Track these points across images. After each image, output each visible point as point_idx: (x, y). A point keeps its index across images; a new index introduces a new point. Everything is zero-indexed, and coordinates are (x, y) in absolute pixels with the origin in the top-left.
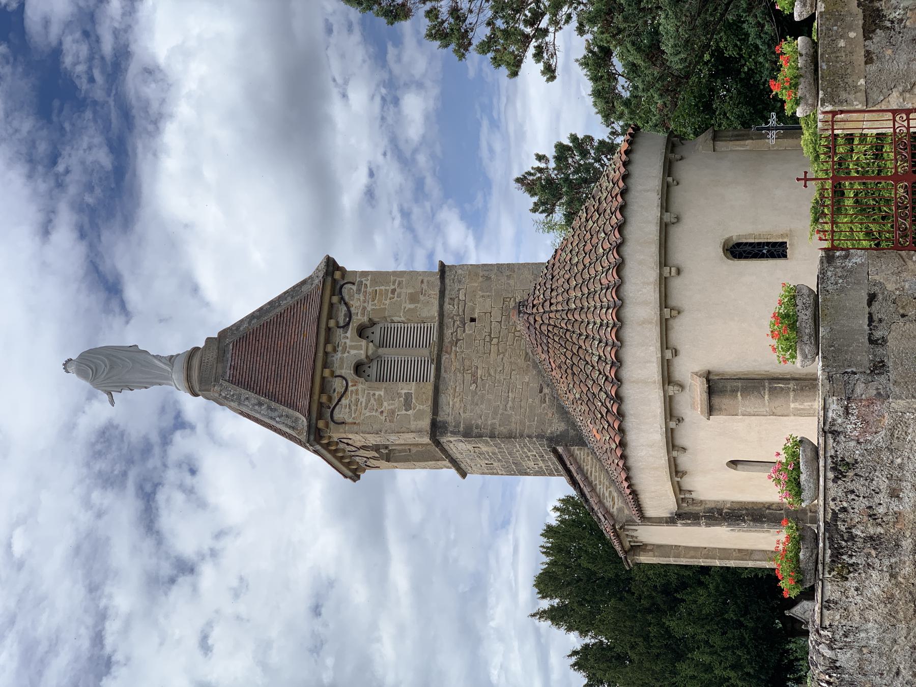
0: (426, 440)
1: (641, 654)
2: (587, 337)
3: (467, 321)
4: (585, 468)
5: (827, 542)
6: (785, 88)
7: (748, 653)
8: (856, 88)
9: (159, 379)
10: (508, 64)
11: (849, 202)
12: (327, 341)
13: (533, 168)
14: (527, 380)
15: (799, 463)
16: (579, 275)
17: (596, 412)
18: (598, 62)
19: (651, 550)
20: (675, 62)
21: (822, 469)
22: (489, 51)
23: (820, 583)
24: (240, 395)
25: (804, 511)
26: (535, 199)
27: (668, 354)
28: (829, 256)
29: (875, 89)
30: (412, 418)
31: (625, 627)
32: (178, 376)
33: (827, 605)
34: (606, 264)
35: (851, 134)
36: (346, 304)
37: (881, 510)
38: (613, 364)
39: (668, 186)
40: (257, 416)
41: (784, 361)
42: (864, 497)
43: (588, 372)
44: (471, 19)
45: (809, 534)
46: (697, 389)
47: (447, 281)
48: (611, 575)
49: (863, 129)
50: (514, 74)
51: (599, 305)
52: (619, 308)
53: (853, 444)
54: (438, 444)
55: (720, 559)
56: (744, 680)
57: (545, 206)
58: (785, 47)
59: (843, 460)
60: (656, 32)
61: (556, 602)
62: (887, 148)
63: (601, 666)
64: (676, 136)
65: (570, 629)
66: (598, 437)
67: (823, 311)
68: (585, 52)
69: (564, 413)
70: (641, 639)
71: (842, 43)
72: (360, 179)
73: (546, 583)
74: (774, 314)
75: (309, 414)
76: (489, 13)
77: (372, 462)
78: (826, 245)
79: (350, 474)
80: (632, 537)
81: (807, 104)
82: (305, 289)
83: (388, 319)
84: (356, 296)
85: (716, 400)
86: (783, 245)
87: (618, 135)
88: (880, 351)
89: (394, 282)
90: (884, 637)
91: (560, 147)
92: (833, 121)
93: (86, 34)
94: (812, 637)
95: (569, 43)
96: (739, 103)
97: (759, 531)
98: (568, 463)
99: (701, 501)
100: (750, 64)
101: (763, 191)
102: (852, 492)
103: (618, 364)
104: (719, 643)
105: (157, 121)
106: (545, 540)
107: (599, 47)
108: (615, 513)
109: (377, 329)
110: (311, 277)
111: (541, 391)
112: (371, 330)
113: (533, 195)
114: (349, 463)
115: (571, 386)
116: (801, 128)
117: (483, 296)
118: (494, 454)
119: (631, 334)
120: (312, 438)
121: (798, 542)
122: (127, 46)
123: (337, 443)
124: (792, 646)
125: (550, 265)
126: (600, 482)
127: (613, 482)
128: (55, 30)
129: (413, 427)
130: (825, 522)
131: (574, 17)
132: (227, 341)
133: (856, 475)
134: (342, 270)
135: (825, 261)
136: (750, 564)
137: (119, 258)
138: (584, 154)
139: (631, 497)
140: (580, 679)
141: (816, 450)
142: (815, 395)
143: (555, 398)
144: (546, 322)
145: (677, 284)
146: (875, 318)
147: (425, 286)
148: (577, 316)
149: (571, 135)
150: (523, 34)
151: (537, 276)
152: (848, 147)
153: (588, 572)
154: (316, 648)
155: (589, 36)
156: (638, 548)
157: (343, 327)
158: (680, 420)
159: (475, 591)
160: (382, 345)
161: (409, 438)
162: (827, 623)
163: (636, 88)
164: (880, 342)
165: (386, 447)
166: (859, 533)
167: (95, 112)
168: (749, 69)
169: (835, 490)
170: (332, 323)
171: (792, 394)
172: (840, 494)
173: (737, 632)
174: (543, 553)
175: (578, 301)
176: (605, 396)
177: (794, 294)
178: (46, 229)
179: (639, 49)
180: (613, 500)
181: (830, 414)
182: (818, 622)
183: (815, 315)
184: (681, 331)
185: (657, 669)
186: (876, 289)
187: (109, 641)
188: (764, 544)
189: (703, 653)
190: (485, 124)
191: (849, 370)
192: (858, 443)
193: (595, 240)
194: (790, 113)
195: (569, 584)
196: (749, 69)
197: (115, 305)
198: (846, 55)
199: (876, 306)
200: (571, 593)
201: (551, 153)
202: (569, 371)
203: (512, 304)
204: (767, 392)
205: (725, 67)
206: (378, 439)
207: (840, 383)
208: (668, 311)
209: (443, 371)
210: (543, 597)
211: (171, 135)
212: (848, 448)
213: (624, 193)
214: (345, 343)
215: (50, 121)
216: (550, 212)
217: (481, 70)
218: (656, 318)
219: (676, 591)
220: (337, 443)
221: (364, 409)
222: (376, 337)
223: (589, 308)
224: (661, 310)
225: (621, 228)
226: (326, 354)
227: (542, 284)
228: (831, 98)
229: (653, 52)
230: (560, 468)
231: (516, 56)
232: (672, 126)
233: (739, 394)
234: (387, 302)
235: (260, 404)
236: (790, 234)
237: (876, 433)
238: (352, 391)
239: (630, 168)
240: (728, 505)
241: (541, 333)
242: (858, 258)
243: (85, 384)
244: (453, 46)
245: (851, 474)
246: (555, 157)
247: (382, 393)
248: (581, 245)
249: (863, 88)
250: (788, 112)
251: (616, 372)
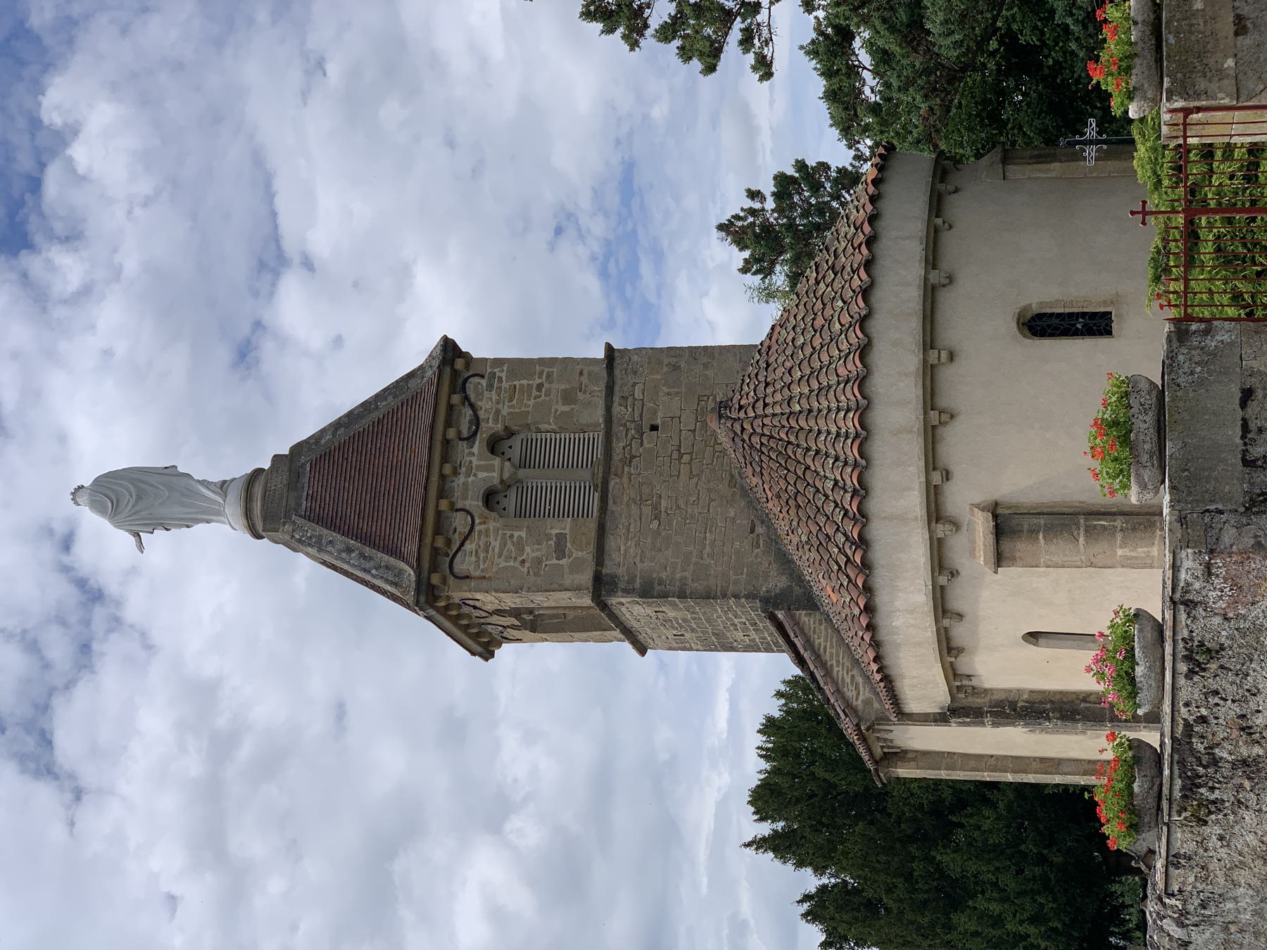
0: (587, 601)
1: (901, 901)
2: (817, 452)
3: (646, 429)
4: (817, 642)
5: (1176, 767)
6: (1112, 74)
7: (1055, 900)
8: (1221, 74)
10: (701, 55)
11: (1207, 248)
12: (445, 459)
13: (742, 209)
14: (732, 514)
15: (1133, 649)
16: (805, 362)
17: (832, 563)
18: (831, 49)
19: (913, 759)
21: (1168, 658)
22: (674, 38)
23: (1165, 828)
24: (320, 538)
26: (746, 254)
27: (936, 478)
28: (1180, 332)
29: (1250, 73)
30: (567, 570)
31: (878, 862)
32: (233, 509)
34: (844, 346)
35: (1210, 145)
36: (472, 406)
38: (855, 492)
39: (936, 231)
40: (346, 567)
41: (1111, 493)
42: (1233, 701)
43: (819, 505)
46: (982, 526)
47: (617, 372)
49: (1232, 136)
50: (710, 69)
51: (834, 405)
52: (863, 412)
53: (1217, 620)
54: (604, 607)
55: (1014, 772)
56: (1048, 938)
57: (759, 265)
59: (1201, 644)
61: (780, 825)
63: (845, 917)
64: (947, 158)
65: (800, 864)
66: (834, 597)
67: (1171, 415)
68: (814, 35)
69: (785, 562)
70: (901, 880)
73: (766, 799)
74: (1096, 421)
75: (419, 565)
77: (511, 633)
78: (1173, 313)
79: (479, 649)
80: (885, 740)
81: (1145, 98)
82: (413, 384)
83: (533, 428)
84: (486, 394)
85: (1006, 545)
86: (1107, 316)
87: (866, 161)
89: (541, 374)
90: (1262, 909)
91: (783, 181)
92: (1185, 124)
96: (1041, 111)
97: (1071, 733)
98: (792, 635)
99: (986, 690)
100: (1057, 55)
102: (1216, 693)
103: (863, 492)
104: (1013, 885)
106: (764, 739)
107: (835, 27)
108: (860, 708)
109: (516, 442)
110: (421, 368)
111: (752, 531)
112: (509, 442)
113: (742, 249)
114: (478, 635)
115: (795, 523)
116: (1133, 142)
117: (668, 394)
118: (685, 620)
119: (881, 448)
120: (422, 599)
121: (1131, 767)
123: (459, 606)
124: (1116, 888)
125: (763, 349)
126: (838, 661)
127: (856, 662)
129: (567, 582)
130: (1172, 738)
132: (303, 459)
133: (1222, 667)
134: (466, 356)
135: (1174, 340)
136: (1057, 779)
138: (816, 187)
139: (882, 684)
140: (815, 935)
142: (1153, 536)
143: (774, 541)
144: (759, 430)
145: (947, 374)
146: (1252, 426)
147: (584, 379)
148: (802, 423)
149: (797, 161)
151: (747, 364)
152: (1205, 169)
153: (821, 785)
156: (898, 755)
157: (467, 439)
158: (954, 574)
160: (523, 464)
162: (1176, 888)
163: (888, 85)
164: (1259, 463)
165: (531, 611)
166: (1225, 755)
168: (1056, 62)
169: (1188, 690)
170: (452, 433)
171: (1119, 536)
172: (1196, 696)
173: (1037, 871)
174: (761, 756)
175: (804, 401)
176: (843, 539)
179: (892, 29)
180: (857, 688)
181: (1183, 575)
182: (1161, 885)
183: (1159, 421)
184: (958, 445)
185: (925, 921)
186: (1253, 382)
188: (1083, 749)
189: (989, 900)
191: (1212, 507)
192: (1226, 619)
193: (829, 312)
194: (1119, 113)
195: (798, 801)
196: (1056, 62)
198: (1205, 22)
199: (1253, 408)
200: (802, 812)
201: (768, 188)
202: (792, 502)
203: (711, 404)
204: (1082, 532)
205: (1021, 60)
206: (518, 600)
208: (935, 417)
209: (610, 501)
210: (761, 819)
212: (1209, 627)
213: (871, 241)
214: (471, 462)
216: (767, 272)
218: (918, 425)
219: (952, 812)
220: (459, 606)
221: (492, 554)
222: (516, 453)
223: (820, 411)
224: (925, 413)
225: (866, 292)
226: (443, 477)
227: (753, 376)
229: (913, 32)
230: (781, 641)
231: (712, 43)
233: (1041, 536)
234: (531, 402)
235: (349, 550)
236: (1116, 299)
237: (1253, 604)
238: (480, 531)
239: (880, 204)
240: (1025, 696)
241: (751, 446)
242: (1224, 334)
245: (1213, 666)
246: (774, 194)
247: (523, 534)
248: (809, 319)
249: (1232, 72)
250: (1117, 111)
251: (860, 503)
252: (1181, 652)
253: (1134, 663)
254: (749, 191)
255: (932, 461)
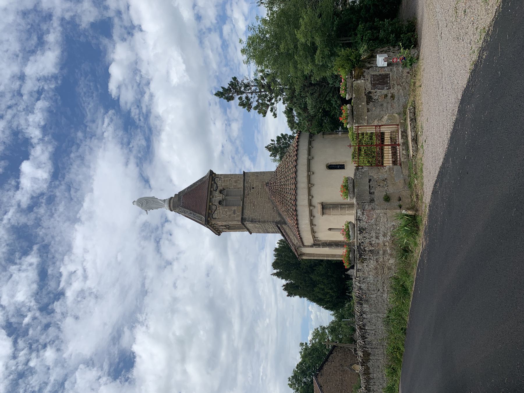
0: (240, 223)
9: (161, 206)
10: (263, 113)
11: (363, 153)
12: (211, 195)
18: (289, 112)
20: (312, 112)
25: (350, 243)
26: (271, 153)
27: (310, 197)
28: (357, 168)
32: (166, 205)
33: (358, 270)
37: (373, 242)
44: (252, 100)
45: (352, 250)
46: (319, 207)
48: (294, 262)
50: (264, 116)
52: (296, 184)
54: (243, 224)
57: (274, 155)
58: (344, 107)
60: (306, 103)
62: (374, 137)
65: (282, 279)
68: (285, 109)
69: (280, 215)
71: (360, 106)
72: (219, 149)
73: (275, 265)
76: (257, 98)
77: (224, 230)
78: (356, 165)
85: (324, 211)
88: (373, 196)
91: (278, 138)
93: (138, 106)
94: (354, 280)
95: (281, 107)
100: (333, 113)
101: (338, 150)
105: (159, 132)
109: (225, 191)
119: (299, 192)
122: (150, 110)
125: (276, 172)
128: (129, 105)
131: (282, 99)
134: (215, 174)
136: (335, 259)
137: (148, 172)
138: (285, 139)
141: (354, 225)
143: (277, 211)
145: (313, 177)
150: (267, 104)
154: (208, 286)
155: (286, 105)
156: (303, 254)
158: (314, 217)
159: (255, 268)
161: (235, 223)
163: (300, 120)
167: (141, 129)
169: (360, 237)
170: (212, 189)
177: (347, 179)
178: (127, 164)
179: (301, 108)
181: (358, 214)
184: (315, 191)
185: (308, 290)
186: (371, 178)
187: (147, 285)
188: (340, 253)
190: (256, 132)
197: (147, 186)
199: (371, 183)
201: (275, 139)
205: (326, 113)
207: (361, 205)
211: (164, 136)
212: (363, 224)
213: (297, 150)
215: (127, 132)
216: (275, 156)
217: (254, 116)
218: (307, 187)
221: (221, 214)
222: (225, 193)
225: (296, 161)
226: (210, 198)
228: (357, 122)
229: (305, 109)
232: (311, 131)
235: (191, 213)
236: (346, 162)
242: (366, 169)
243: (139, 208)
244: (246, 108)
245: (364, 232)
250: (345, 127)
252: (358, 229)
253: (349, 232)
254: (219, 94)
255: (309, 194)
